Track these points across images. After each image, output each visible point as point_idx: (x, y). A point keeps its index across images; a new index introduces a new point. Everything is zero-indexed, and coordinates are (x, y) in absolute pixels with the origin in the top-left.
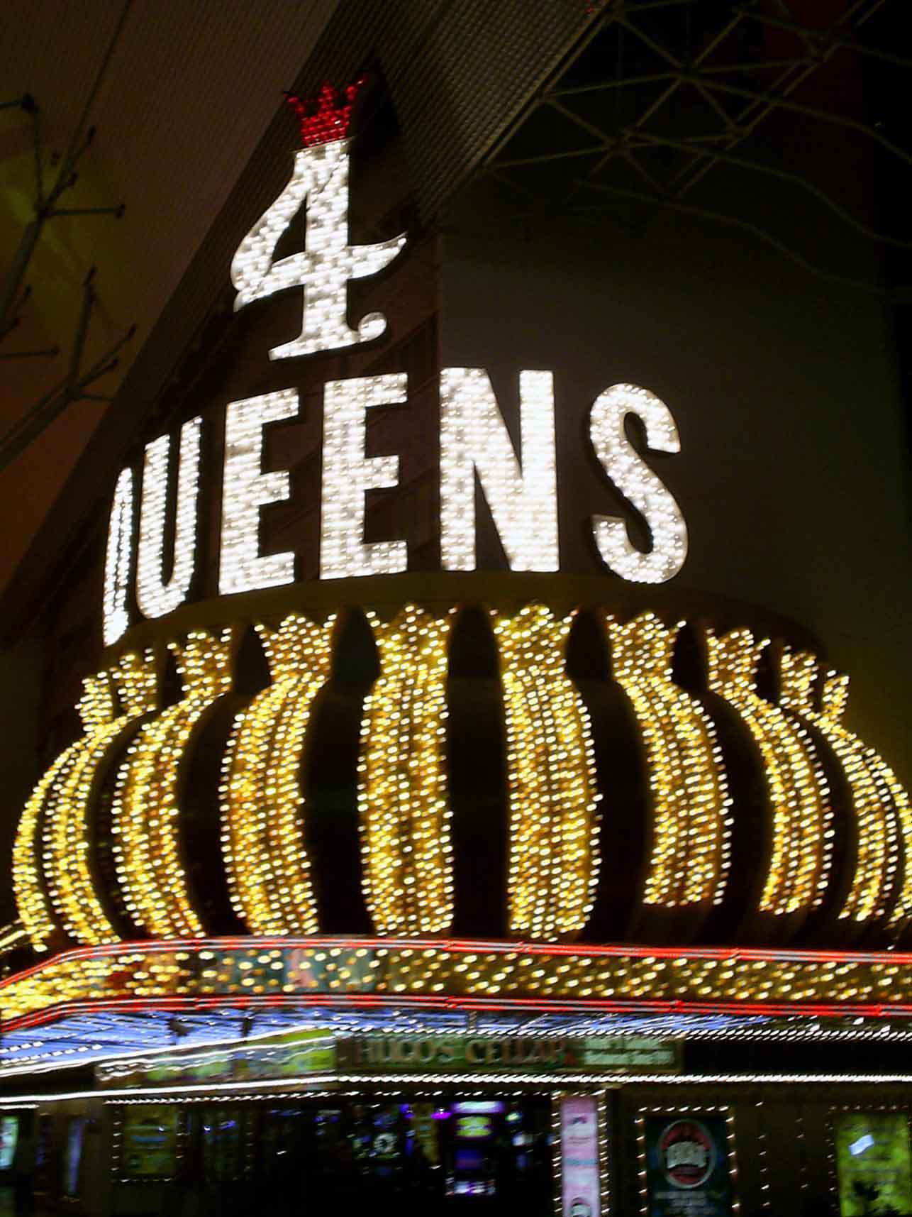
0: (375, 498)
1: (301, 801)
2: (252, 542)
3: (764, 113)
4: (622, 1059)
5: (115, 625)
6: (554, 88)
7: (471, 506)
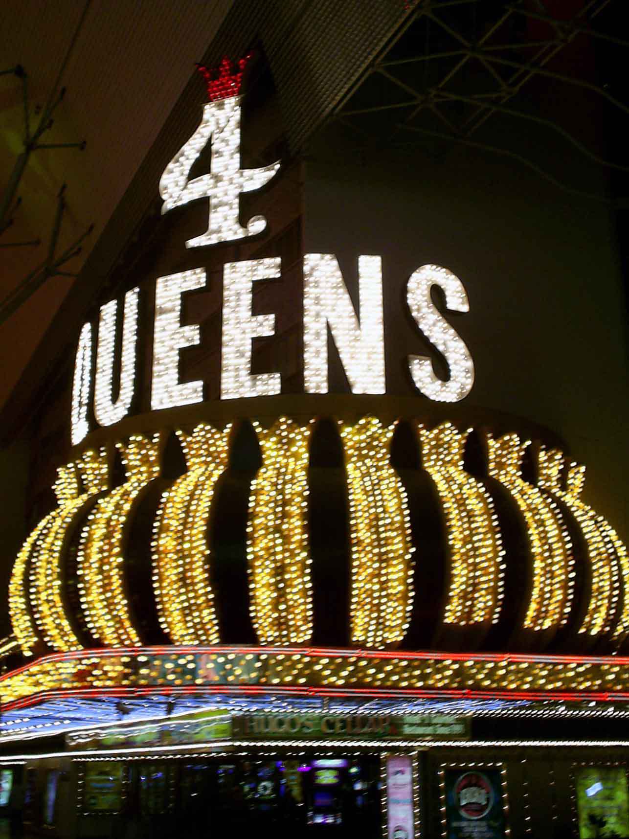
0: (258, 343)
1: (208, 552)
2: (174, 374)
3: (527, 78)
4: (429, 730)
5: (79, 431)
6: (382, 60)
7: (325, 349)
